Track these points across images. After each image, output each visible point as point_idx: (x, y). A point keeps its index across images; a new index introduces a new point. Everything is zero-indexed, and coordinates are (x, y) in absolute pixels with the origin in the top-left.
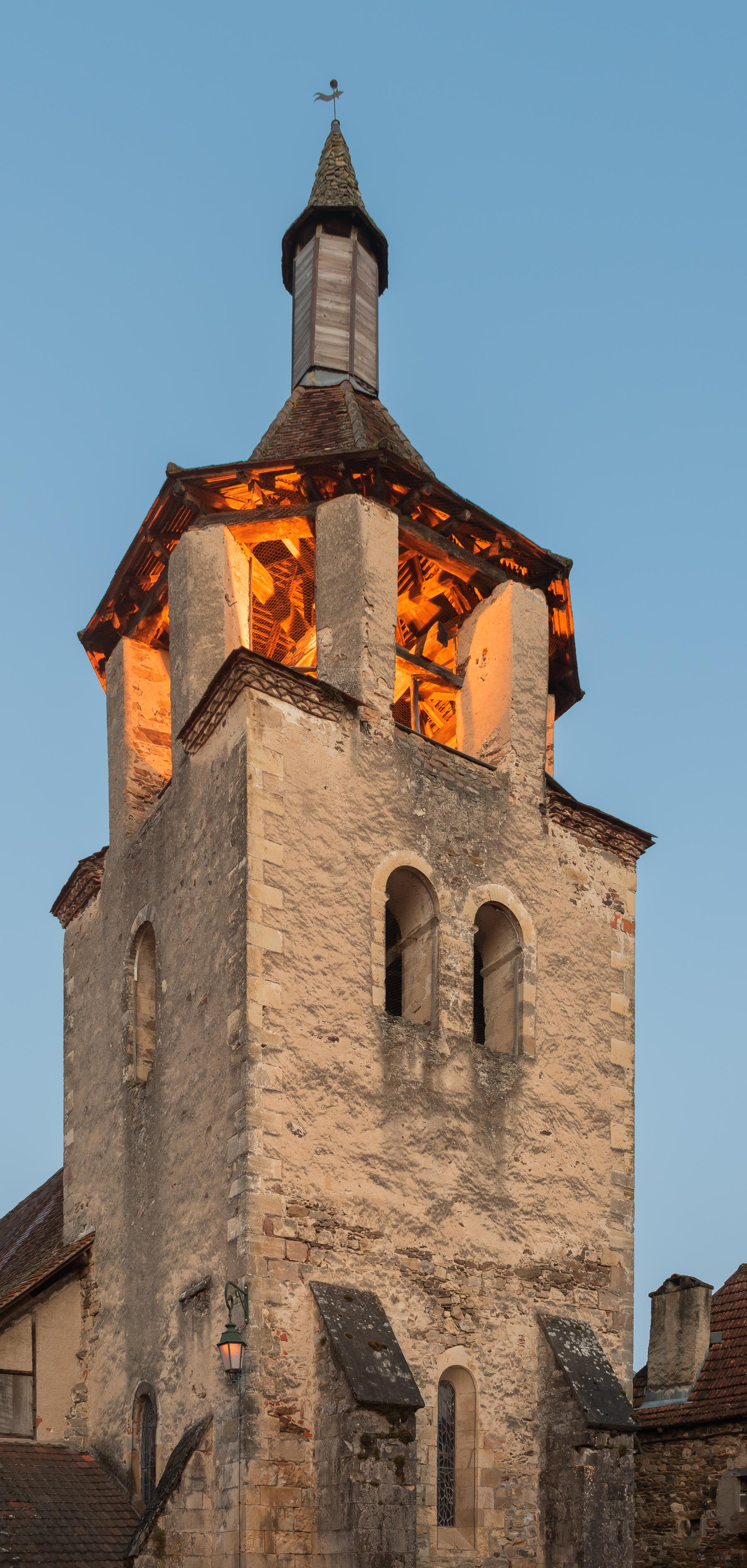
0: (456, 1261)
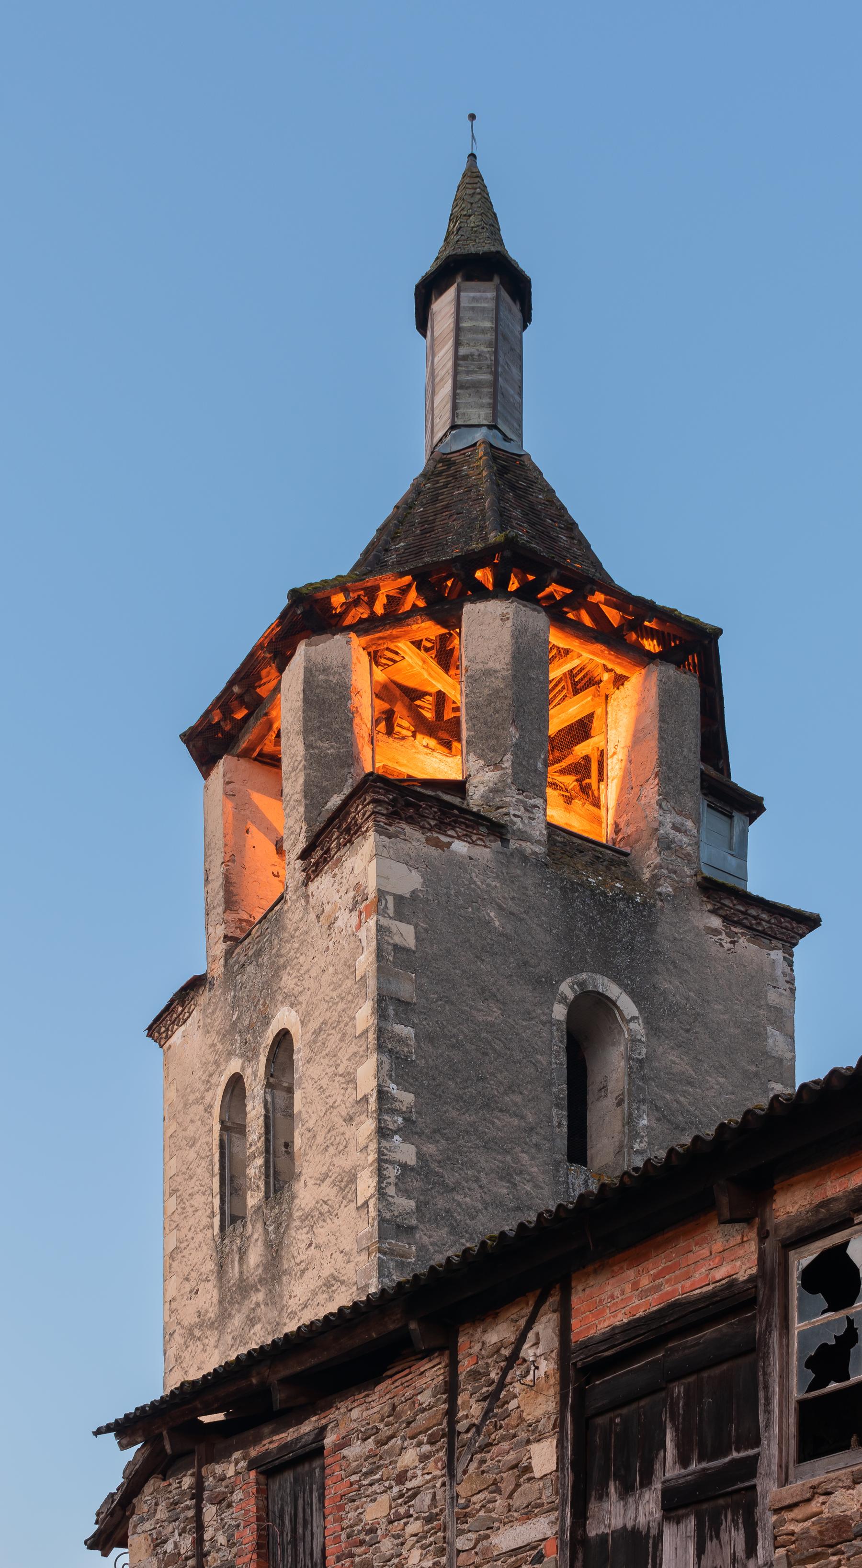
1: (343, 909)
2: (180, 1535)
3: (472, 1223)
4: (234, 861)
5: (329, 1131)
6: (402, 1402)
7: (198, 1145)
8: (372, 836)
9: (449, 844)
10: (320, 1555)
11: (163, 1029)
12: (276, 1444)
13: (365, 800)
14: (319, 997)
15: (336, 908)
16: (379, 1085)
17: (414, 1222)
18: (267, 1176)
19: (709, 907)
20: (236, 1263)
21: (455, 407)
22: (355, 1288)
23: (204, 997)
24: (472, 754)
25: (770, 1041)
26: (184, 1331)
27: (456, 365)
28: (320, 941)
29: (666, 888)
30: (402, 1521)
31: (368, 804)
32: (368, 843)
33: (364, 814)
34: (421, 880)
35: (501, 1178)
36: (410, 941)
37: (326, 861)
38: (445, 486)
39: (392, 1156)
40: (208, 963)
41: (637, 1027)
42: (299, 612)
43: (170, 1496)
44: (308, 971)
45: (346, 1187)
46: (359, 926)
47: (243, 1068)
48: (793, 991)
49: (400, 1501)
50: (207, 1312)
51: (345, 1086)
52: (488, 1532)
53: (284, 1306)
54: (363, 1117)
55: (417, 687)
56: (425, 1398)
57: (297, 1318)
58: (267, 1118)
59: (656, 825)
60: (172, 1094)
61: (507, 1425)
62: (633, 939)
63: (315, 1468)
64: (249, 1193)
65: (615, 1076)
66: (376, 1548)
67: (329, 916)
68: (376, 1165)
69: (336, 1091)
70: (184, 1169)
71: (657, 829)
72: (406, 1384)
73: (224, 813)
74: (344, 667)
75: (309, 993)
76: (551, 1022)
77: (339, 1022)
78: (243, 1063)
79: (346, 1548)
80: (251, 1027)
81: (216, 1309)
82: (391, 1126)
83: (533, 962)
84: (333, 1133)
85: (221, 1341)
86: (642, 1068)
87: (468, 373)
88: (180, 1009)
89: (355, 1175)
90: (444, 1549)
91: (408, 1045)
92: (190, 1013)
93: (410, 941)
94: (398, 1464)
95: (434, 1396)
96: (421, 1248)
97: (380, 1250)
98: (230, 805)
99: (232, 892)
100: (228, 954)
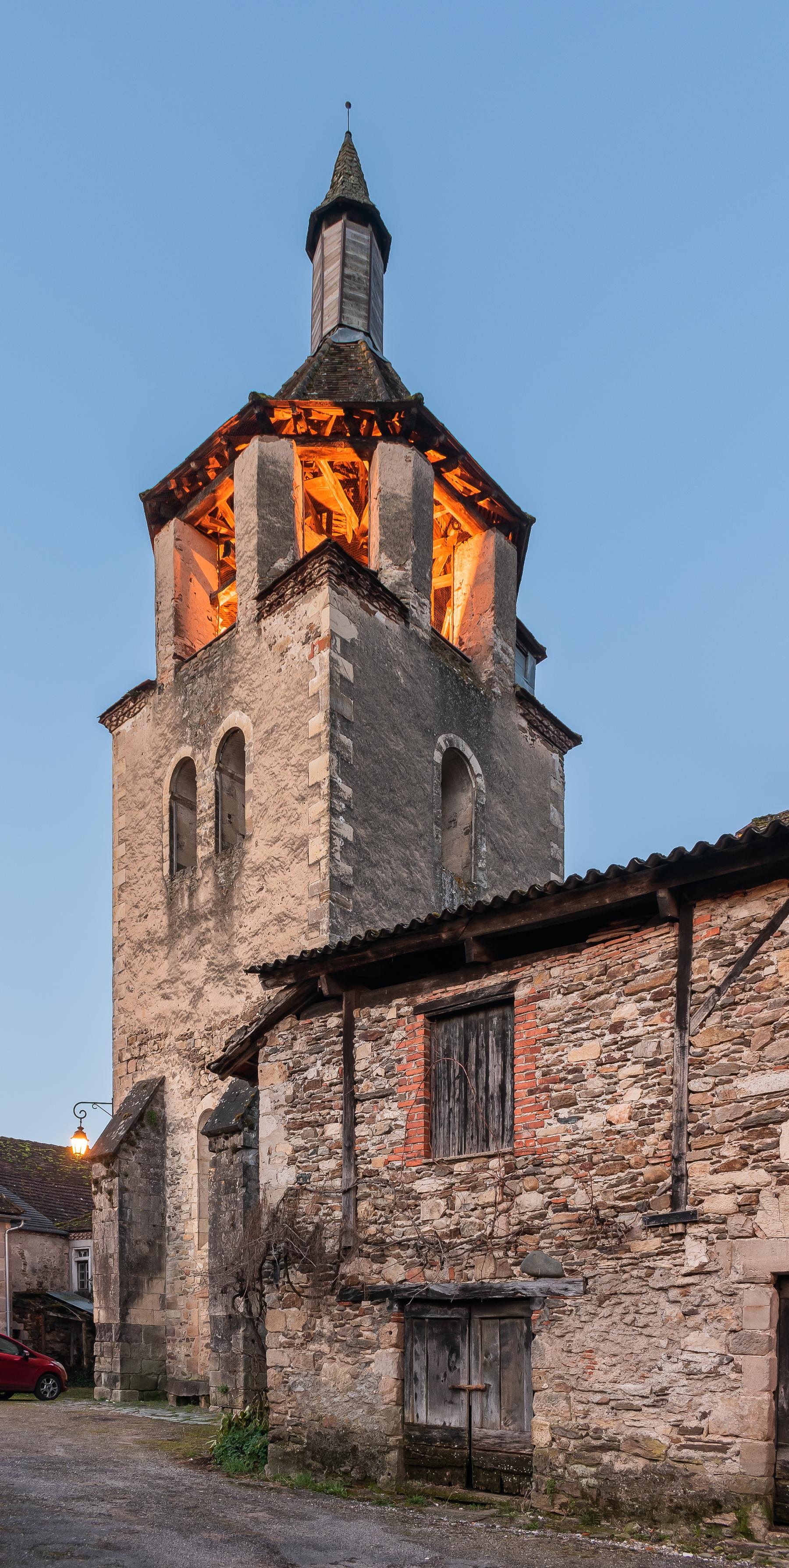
0: (206, 1030)
1: (295, 642)
2: (323, 1065)
3: (386, 893)
4: (181, 600)
5: (281, 806)
6: (618, 964)
7: (148, 808)
8: (326, 590)
9: (375, 613)
10: (497, 1089)
11: (114, 718)
12: (451, 994)
13: (322, 559)
14: (272, 706)
15: (288, 640)
16: (331, 776)
17: (351, 883)
18: (217, 836)
19: (521, 711)
20: (186, 898)
21: (341, 311)
22: (306, 924)
23: (154, 698)
24: (383, 554)
25: (552, 814)
26: (133, 944)
28: (272, 665)
29: (497, 690)
30: (616, 1065)
31: (325, 563)
32: (324, 594)
33: (319, 571)
34: (357, 632)
35: (404, 865)
36: (351, 677)
37: (279, 604)
38: (341, 363)
39: (338, 830)
40: (158, 673)
41: (481, 781)
42: (256, 412)
43: (311, 1032)
44: (260, 686)
45: (298, 848)
46: (312, 656)
47: (194, 754)
48: (564, 784)
49: (613, 1047)
50: (156, 932)
51: (297, 774)
52: (732, 1077)
53: (234, 933)
54: (315, 798)
55: (324, 503)
56: (651, 962)
57: (247, 943)
58: (217, 793)
59: (492, 644)
60: (122, 768)
61: (760, 988)
62: (479, 719)
63: (492, 1018)
64: (199, 847)
65: (463, 813)
66: (581, 1085)
67: (281, 646)
68: (328, 834)
69: (288, 777)
70: (133, 825)
71: (492, 647)
72: (622, 949)
73: (174, 561)
74: (289, 464)
75: (261, 702)
76: (432, 762)
77: (291, 726)
78: (194, 750)
79: (541, 1084)
80: (201, 724)
81: (166, 930)
82: (338, 808)
83: (423, 716)
84: (285, 808)
85: (171, 954)
86: (483, 811)
87: (351, 289)
88: (132, 704)
89: (307, 841)
90: (671, 1090)
91: (348, 752)
92: (140, 709)
94: (612, 1016)
95: (662, 960)
96: (356, 903)
97: (331, 898)
98: (179, 556)
99: (180, 623)
100: (177, 668)
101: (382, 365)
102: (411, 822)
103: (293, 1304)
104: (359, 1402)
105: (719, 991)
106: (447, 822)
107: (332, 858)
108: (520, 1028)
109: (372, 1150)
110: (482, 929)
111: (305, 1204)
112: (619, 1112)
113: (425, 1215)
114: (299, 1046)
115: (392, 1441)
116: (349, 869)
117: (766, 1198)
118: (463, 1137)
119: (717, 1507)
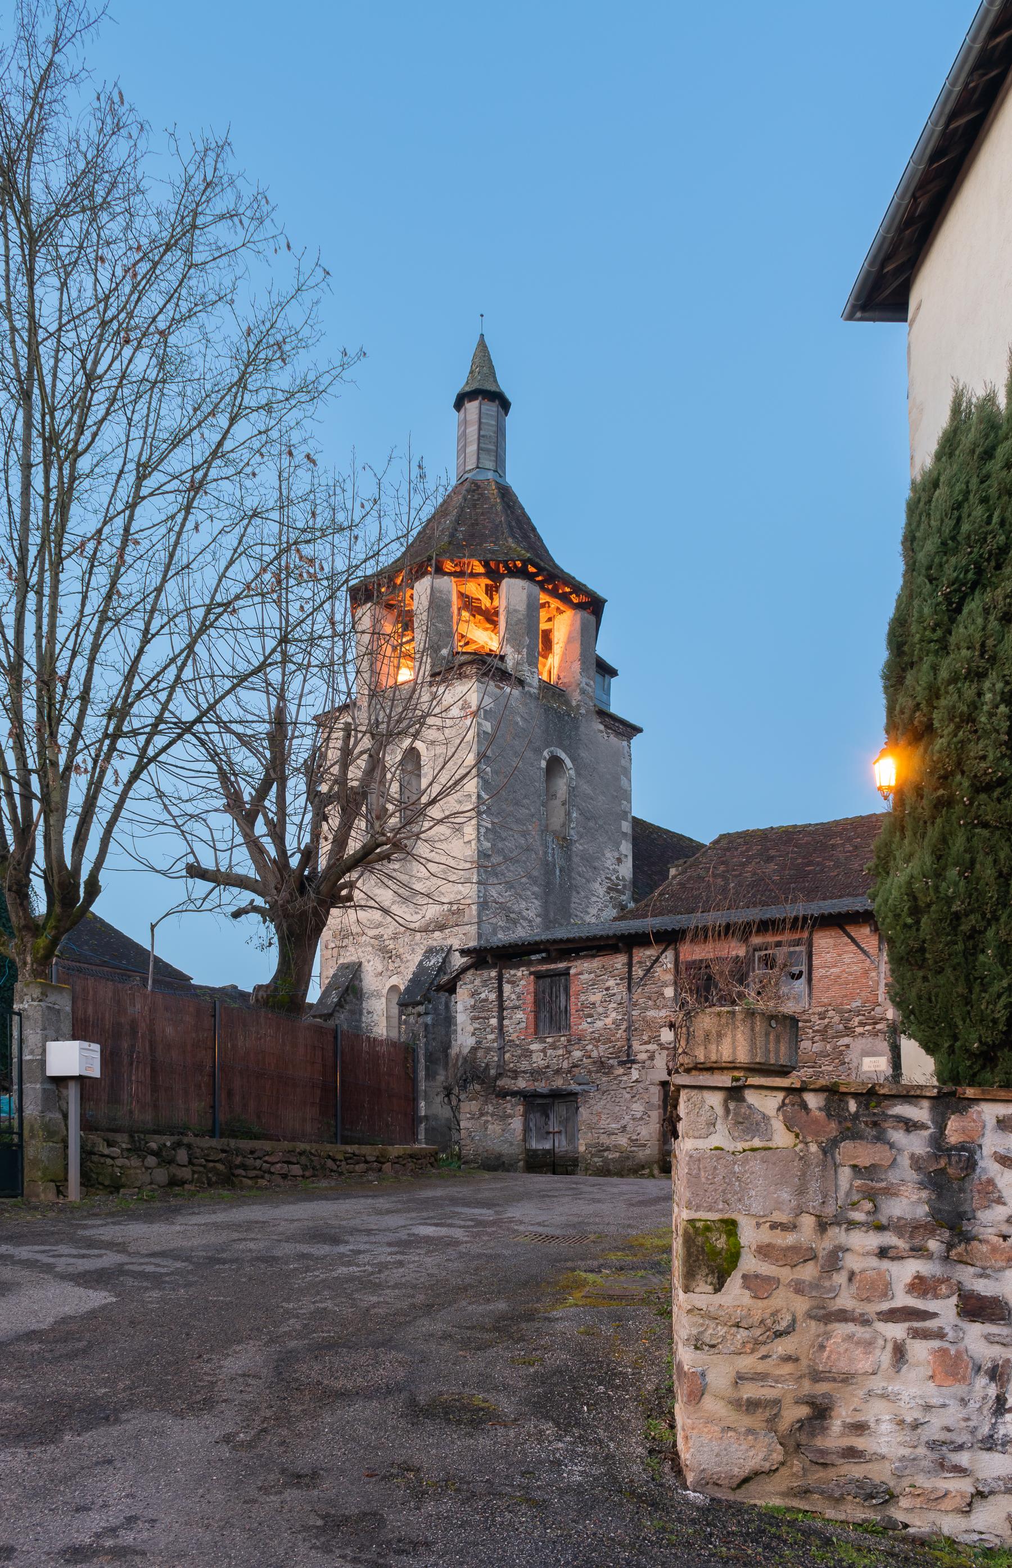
21: (478, 458)
27: (479, 439)
29: (583, 711)
38: (478, 500)
76: (540, 768)
93: (489, 730)
101: (506, 493)
102: (527, 808)
103: (474, 1099)
104: (506, 1141)
105: (641, 979)
106: (551, 795)
107: (479, 840)
108: (572, 986)
109: (511, 1031)
110: (556, 947)
111: (480, 1054)
112: (609, 1021)
113: (534, 1060)
114: (477, 982)
115: (520, 1157)
116: (489, 845)
117: (656, 1054)
118: (550, 1027)
119: (643, 1167)
